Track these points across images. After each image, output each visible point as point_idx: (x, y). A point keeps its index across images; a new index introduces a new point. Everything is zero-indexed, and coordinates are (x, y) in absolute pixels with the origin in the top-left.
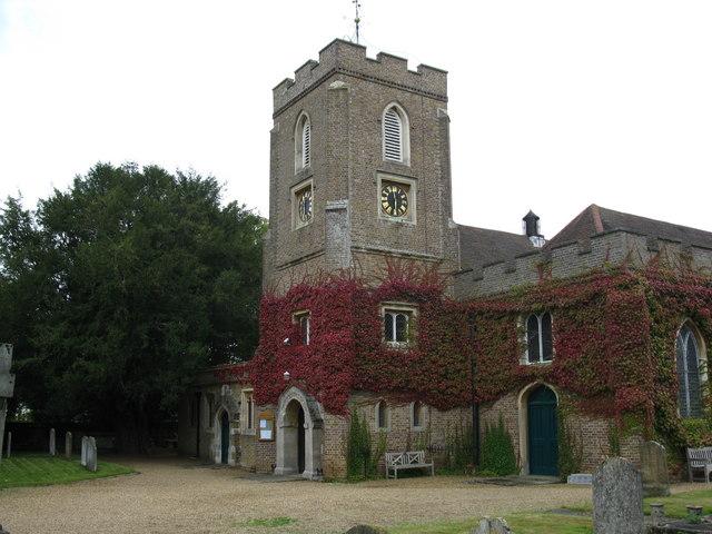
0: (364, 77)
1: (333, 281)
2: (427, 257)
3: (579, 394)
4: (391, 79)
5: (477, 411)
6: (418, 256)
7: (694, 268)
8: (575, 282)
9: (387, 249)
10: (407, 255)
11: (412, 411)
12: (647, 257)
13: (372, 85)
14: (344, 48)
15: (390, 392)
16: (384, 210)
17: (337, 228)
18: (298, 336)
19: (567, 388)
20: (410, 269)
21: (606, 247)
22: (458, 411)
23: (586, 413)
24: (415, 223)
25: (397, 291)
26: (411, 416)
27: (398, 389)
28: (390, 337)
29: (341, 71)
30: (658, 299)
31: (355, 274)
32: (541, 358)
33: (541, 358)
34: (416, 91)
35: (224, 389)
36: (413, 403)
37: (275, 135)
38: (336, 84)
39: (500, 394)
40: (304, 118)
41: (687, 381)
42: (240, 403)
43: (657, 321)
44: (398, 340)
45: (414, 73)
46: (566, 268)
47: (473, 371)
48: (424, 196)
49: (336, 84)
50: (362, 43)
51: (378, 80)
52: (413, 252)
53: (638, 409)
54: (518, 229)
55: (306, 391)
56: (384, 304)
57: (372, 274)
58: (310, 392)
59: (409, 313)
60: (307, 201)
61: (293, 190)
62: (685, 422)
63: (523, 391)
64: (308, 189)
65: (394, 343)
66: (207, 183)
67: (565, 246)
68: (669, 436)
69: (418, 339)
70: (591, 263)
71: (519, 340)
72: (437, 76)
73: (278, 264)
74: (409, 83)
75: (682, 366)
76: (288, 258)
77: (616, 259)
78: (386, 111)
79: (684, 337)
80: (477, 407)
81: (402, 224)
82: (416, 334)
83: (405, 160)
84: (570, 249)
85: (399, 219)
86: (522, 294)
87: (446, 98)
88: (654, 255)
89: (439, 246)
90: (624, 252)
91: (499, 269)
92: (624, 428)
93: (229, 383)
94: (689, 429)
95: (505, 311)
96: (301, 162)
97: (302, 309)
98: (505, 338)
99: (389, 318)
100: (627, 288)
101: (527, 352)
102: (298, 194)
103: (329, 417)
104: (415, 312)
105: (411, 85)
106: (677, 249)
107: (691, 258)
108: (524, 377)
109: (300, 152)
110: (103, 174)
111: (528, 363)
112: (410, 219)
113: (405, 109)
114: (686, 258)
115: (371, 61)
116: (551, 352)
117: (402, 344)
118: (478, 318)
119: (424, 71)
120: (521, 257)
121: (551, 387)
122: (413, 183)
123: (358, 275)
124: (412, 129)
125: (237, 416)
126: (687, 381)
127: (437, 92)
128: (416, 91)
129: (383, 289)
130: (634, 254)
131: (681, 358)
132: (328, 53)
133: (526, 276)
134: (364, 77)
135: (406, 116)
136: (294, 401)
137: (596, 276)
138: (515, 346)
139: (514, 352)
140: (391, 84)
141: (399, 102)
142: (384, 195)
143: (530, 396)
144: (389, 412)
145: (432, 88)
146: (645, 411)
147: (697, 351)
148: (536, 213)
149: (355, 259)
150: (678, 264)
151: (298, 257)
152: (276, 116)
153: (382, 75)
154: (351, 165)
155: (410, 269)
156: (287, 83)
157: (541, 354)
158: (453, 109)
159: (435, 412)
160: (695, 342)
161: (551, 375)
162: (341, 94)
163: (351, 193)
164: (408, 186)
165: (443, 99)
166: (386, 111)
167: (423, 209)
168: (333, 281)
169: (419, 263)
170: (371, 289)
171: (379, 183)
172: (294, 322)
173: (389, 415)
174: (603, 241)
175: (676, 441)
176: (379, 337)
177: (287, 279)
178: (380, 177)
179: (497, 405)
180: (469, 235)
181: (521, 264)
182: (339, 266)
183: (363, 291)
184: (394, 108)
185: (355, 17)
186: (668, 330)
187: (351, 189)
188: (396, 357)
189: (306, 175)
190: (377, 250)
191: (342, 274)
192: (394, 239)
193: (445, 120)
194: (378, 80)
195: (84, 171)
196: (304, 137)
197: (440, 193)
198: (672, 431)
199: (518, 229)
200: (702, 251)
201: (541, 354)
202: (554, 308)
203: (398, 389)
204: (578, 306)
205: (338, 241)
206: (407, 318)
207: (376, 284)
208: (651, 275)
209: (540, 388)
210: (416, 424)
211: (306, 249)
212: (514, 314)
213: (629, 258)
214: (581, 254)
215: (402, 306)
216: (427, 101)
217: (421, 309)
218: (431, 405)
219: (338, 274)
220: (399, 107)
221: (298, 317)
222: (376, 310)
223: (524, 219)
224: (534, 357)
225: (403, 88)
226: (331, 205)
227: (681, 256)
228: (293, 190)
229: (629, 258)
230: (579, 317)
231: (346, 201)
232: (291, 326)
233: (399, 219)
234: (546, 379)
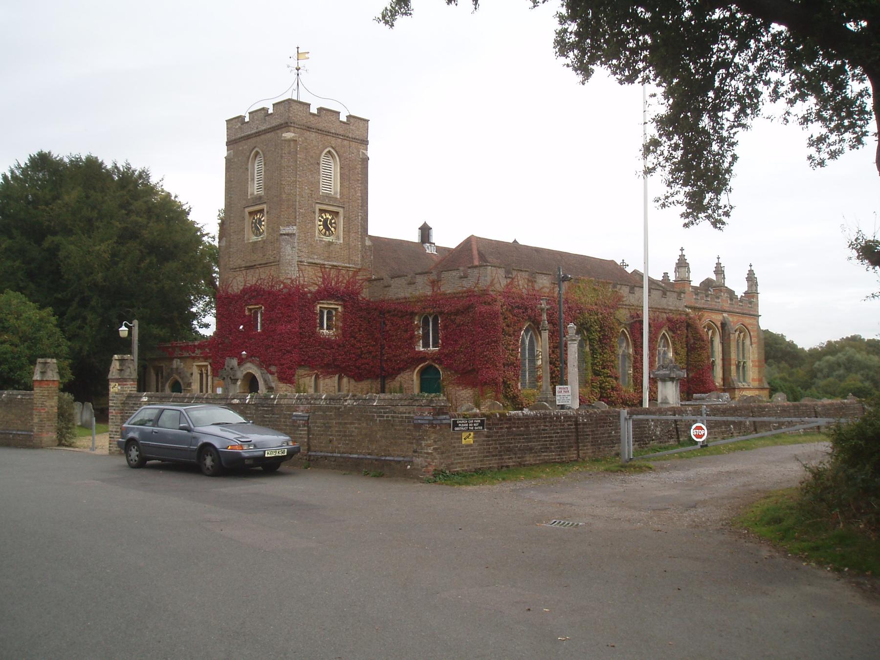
0: (309, 128)
1: (285, 287)
2: (350, 267)
3: (456, 372)
4: (327, 129)
5: (384, 382)
6: (343, 267)
7: (537, 288)
8: (454, 296)
9: (321, 262)
10: (336, 266)
11: (336, 381)
12: (504, 282)
13: (314, 135)
14: (295, 107)
15: (322, 367)
16: (320, 231)
17: (289, 248)
18: (251, 323)
19: (448, 367)
20: (337, 276)
21: (478, 275)
22: (369, 381)
23: (459, 384)
24: (342, 241)
25: (327, 293)
26: (336, 385)
27: (328, 365)
28: (322, 327)
29: (292, 125)
30: (510, 311)
31: (299, 282)
32: (431, 346)
33: (431, 346)
34: (345, 138)
35: (176, 363)
36: (337, 376)
37: (228, 160)
38: (288, 135)
39: (400, 370)
40: (257, 154)
41: (527, 365)
42: (192, 374)
43: (508, 326)
44: (327, 329)
45: (344, 123)
46: (451, 285)
47: (381, 352)
48: (348, 220)
49: (288, 135)
50: (302, 99)
51: (319, 131)
52: (340, 264)
53: (494, 383)
54: (414, 237)
55: (260, 366)
56: (319, 303)
57: (311, 280)
58: (262, 367)
59: (336, 309)
60: (260, 221)
61: (247, 210)
62: (524, 392)
63: (420, 366)
64: (261, 211)
65: (325, 331)
66: (140, 176)
67: (451, 270)
68: (513, 401)
69: (343, 329)
70: (467, 284)
71: (416, 333)
72: (361, 124)
73: (231, 266)
74: (341, 131)
75: (523, 354)
76: (244, 264)
77: (483, 285)
78: (324, 152)
79: (527, 335)
80: (734, 389)
81: (332, 243)
82: (341, 325)
83: (336, 193)
84: (454, 273)
85: (330, 239)
86: (419, 300)
87: (367, 141)
88: (509, 280)
89: (358, 258)
90: (489, 279)
91: (403, 281)
92: (483, 394)
93: (180, 358)
94: (527, 396)
95: (407, 312)
96: (255, 189)
97: (255, 305)
98: (406, 331)
99: (322, 312)
100: (489, 304)
101: (421, 341)
102: (251, 213)
103: (281, 385)
104: (340, 309)
105: (342, 133)
106: (525, 275)
107: (535, 281)
108: (421, 357)
109: (253, 179)
110: (42, 161)
111: (422, 349)
112: (338, 238)
113: (337, 152)
114: (532, 281)
115: (314, 115)
116: (438, 342)
117: (331, 332)
118: (386, 315)
119: (352, 120)
120: (420, 274)
121: (437, 366)
122: (341, 210)
123: (302, 282)
124: (341, 168)
125: (189, 385)
126: (527, 365)
127: (361, 138)
128: (345, 138)
129: (318, 292)
130: (496, 280)
131: (523, 349)
132: (282, 108)
133: (422, 289)
134: (309, 128)
135: (338, 163)
136: (249, 374)
137: (470, 293)
138: (412, 337)
139: (411, 340)
140: (328, 133)
141: (333, 148)
142: (320, 221)
143: (422, 373)
144: (321, 382)
145: (357, 134)
146: (496, 384)
147: (535, 344)
148: (430, 225)
149: (300, 270)
150: (526, 286)
151: (253, 264)
152: (229, 143)
153: (321, 126)
154: (298, 198)
155: (337, 276)
156: (240, 119)
157: (431, 343)
158: (372, 151)
159: (352, 382)
160: (534, 337)
161: (437, 358)
162: (292, 144)
163: (297, 221)
164: (337, 213)
165: (365, 142)
166: (324, 152)
167: (347, 231)
168: (285, 287)
169: (344, 272)
170: (310, 292)
171: (317, 211)
172: (247, 313)
173: (321, 385)
174: (476, 271)
175: (516, 404)
176: (316, 327)
177: (240, 279)
178: (318, 207)
179: (398, 378)
180: (378, 241)
181: (420, 279)
182: (289, 276)
183: (305, 293)
184: (329, 152)
185: (296, 66)
186: (515, 331)
187: (297, 217)
188: (327, 342)
189: (259, 200)
190: (315, 263)
191: (292, 282)
192: (326, 254)
193: (366, 160)
194: (319, 131)
195: (24, 161)
196: (257, 168)
197: (360, 218)
198: (514, 397)
199: (414, 237)
200: (543, 276)
201: (431, 343)
202: (441, 313)
203: (328, 365)
204: (458, 312)
205: (289, 257)
206: (334, 313)
207: (314, 289)
208: (507, 294)
209: (429, 367)
210: (339, 390)
211: (257, 258)
212: (413, 314)
213: (492, 284)
214: (461, 278)
215: (331, 304)
216: (353, 144)
217: (344, 307)
218: (348, 376)
219: (289, 282)
220: (333, 151)
221: (250, 310)
222: (313, 307)
223: (419, 229)
224: (426, 345)
225: (336, 135)
226: (284, 230)
227: (529, 281)
228: (247, 210)
229: (492, 284)
230: (457, 321)
231: (295, 227)
232: (245, 316)
233: (330, 239)
234: (434, 361)
